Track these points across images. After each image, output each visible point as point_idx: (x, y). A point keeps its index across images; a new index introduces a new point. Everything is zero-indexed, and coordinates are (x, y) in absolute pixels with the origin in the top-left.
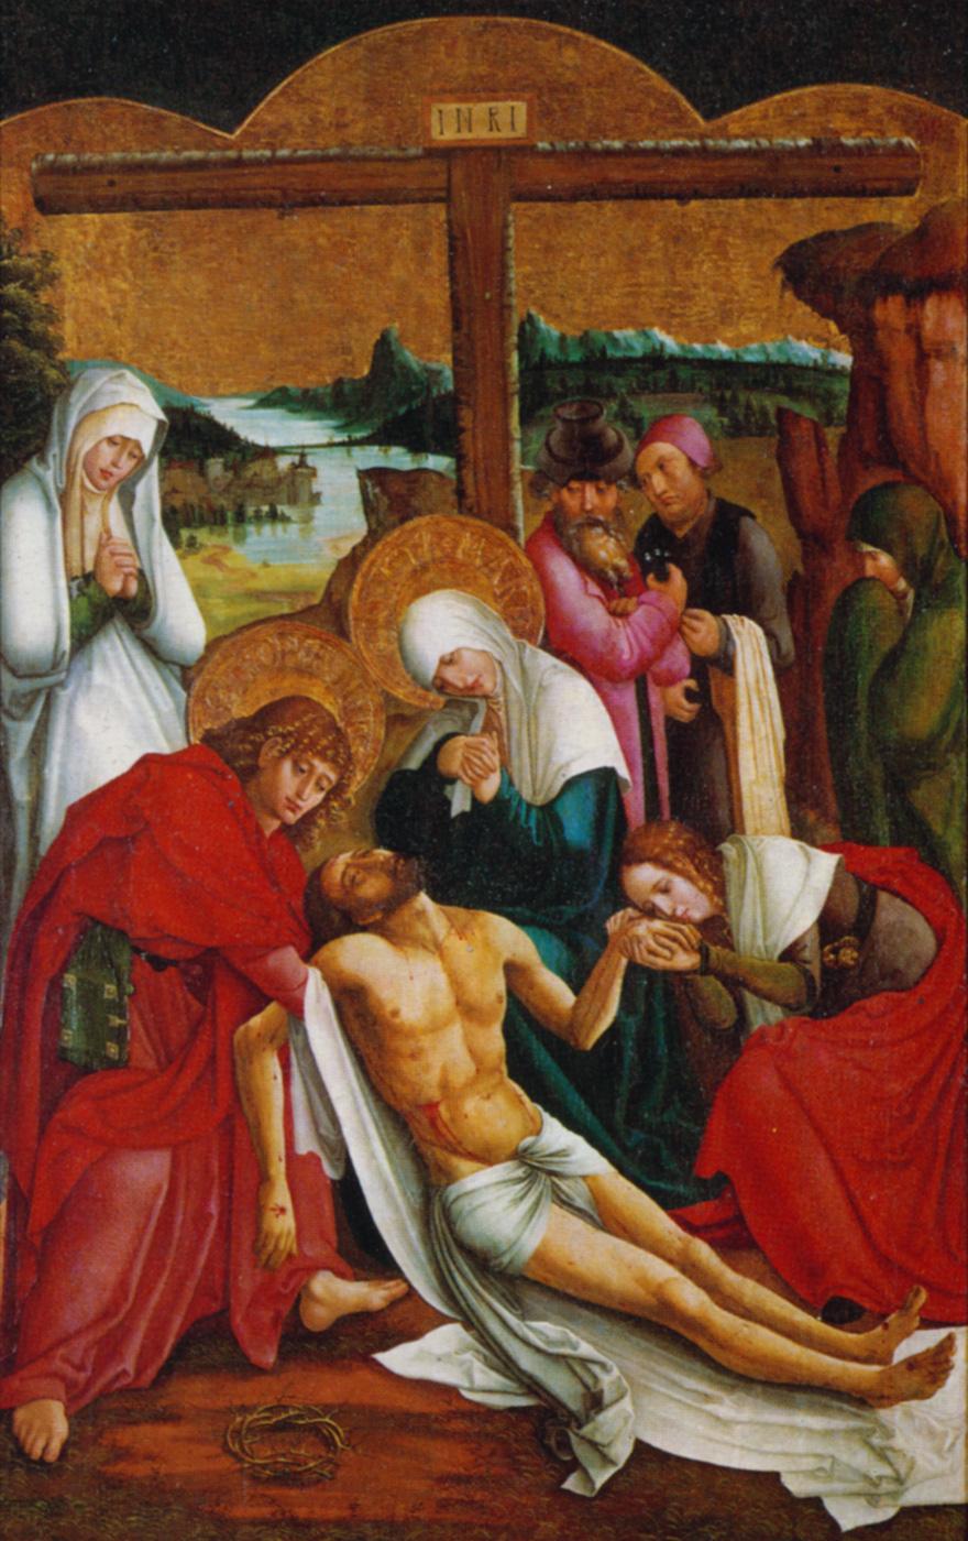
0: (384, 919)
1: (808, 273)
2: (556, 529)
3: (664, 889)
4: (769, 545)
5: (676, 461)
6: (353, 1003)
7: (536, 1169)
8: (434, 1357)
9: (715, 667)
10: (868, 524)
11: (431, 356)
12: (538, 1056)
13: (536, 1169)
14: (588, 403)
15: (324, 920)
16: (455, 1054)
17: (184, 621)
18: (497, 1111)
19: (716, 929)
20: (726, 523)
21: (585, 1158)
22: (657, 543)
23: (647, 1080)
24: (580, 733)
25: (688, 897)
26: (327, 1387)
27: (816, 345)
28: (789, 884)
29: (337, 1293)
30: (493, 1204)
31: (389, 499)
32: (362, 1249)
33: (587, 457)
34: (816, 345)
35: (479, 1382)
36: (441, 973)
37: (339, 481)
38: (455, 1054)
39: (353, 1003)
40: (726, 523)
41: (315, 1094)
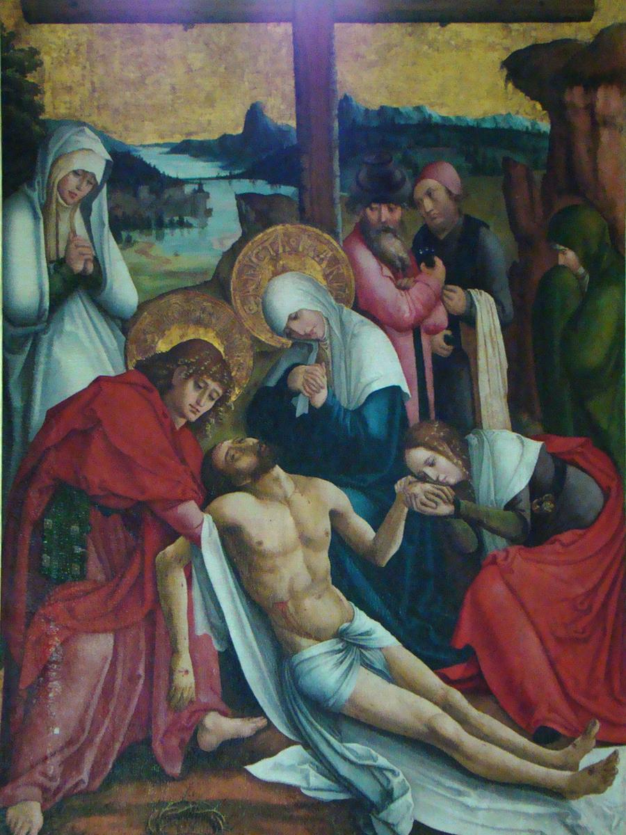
0: (251, 482)
1: (519, 69)
2: (366, 234)
3: (433, 463)
4: (498, 244)
5: (440, 188)
6: (232, 537)
7: (350, 644)
8: (284, 768)
9: (463, 323)
10: (560, 232)
11: (281, 112)
12: (350, 568)
13: (350, 644)
14: (389, 148)
15: (214, 483)
16: (298, 571)
17: (124, 289)
18: (327, 607)
19: (464, 489)
20: (471, 229)
21: (382, 637)
22: (426, 244)
23: (423, 587)
24: (379, 364)
25: (446, 469)
26: (213, 789)
27: (526, 113)
28: (512, 460)
29: (222, 726)
30: (323, 667)
31: (255, 214)
32: (239, 699)
33: (384, 189)
34: (526, 113)
35: (314, 784)
36: (291, 518)
37: (223, 201)
38: (298, 571)
39: (232, 537)
40: (471, 229)
41: (206, 598)
